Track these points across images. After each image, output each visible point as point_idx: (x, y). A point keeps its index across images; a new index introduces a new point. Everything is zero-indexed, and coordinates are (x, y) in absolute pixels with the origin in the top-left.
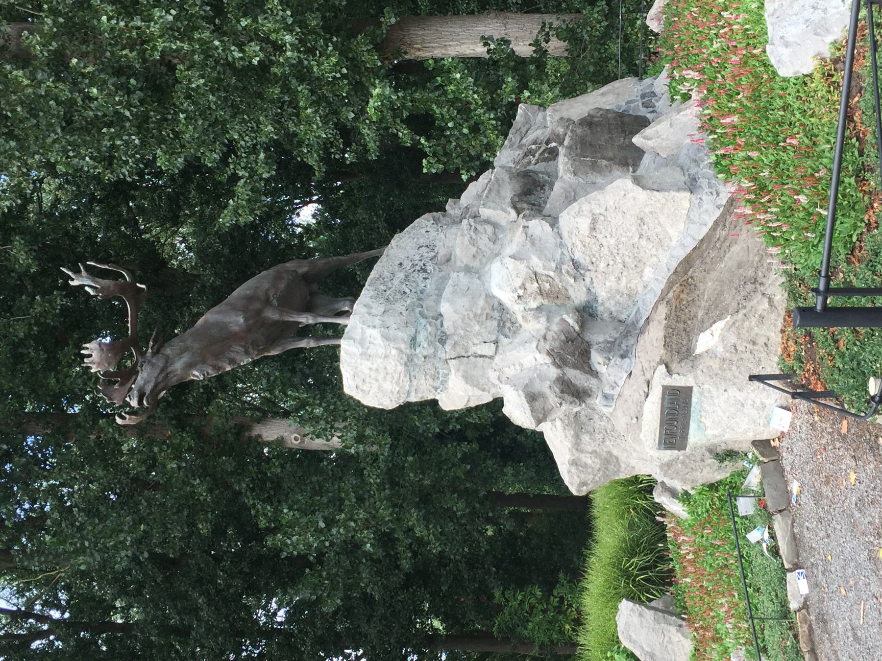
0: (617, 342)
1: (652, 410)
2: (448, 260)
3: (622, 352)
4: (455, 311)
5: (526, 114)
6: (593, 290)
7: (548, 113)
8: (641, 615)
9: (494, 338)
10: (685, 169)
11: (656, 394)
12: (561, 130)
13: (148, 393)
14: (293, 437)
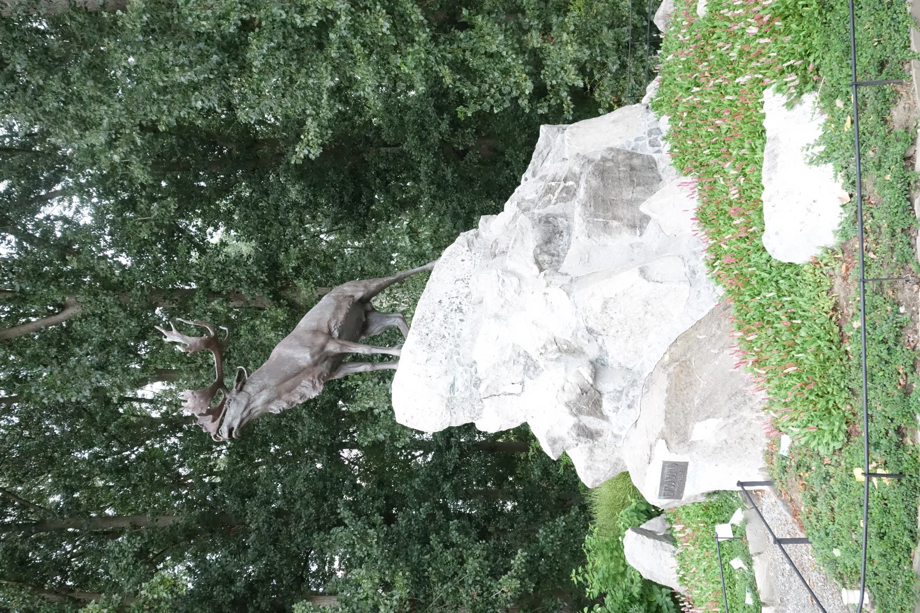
0: (625, 392)
2: (481, 302)
3: (629, 402)
5: (547, 137)
7: (567, 137)
9: (520, 380)
10: (686, 259)
12: (577, 169)
13: (235, 428)
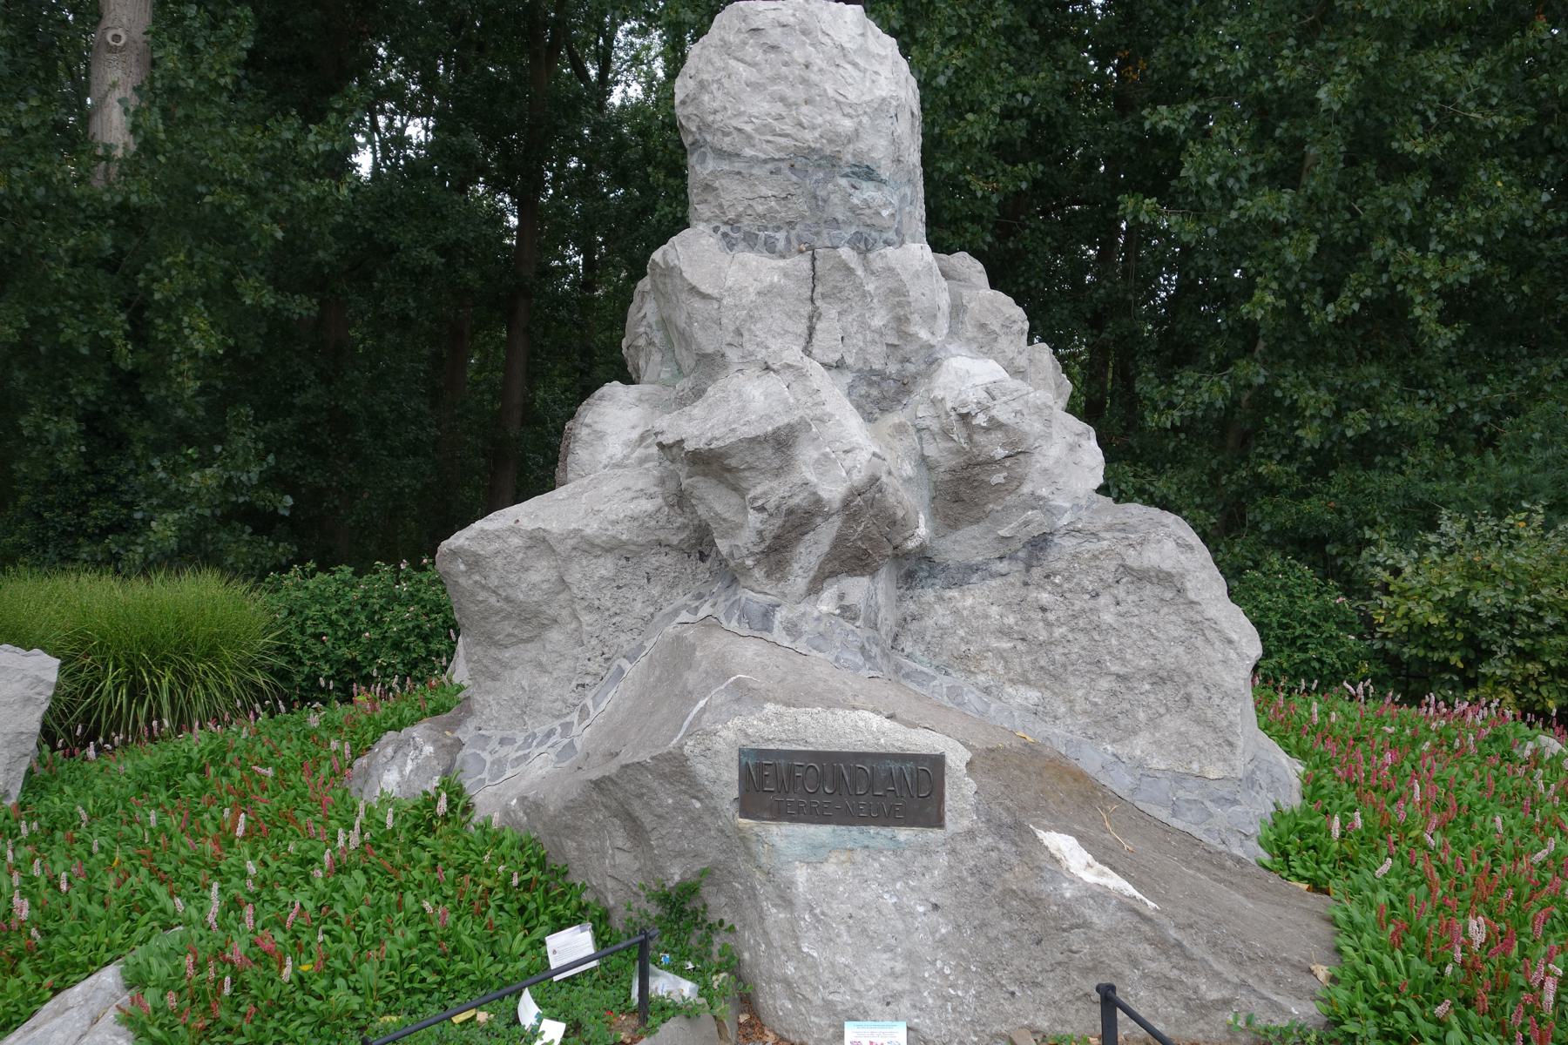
1: (865, 727)
4: (917, 275)
6: (975, 578)
8: (27, 700)
9: (849, 361)
11: (922, 741)
14: (120, 32)
